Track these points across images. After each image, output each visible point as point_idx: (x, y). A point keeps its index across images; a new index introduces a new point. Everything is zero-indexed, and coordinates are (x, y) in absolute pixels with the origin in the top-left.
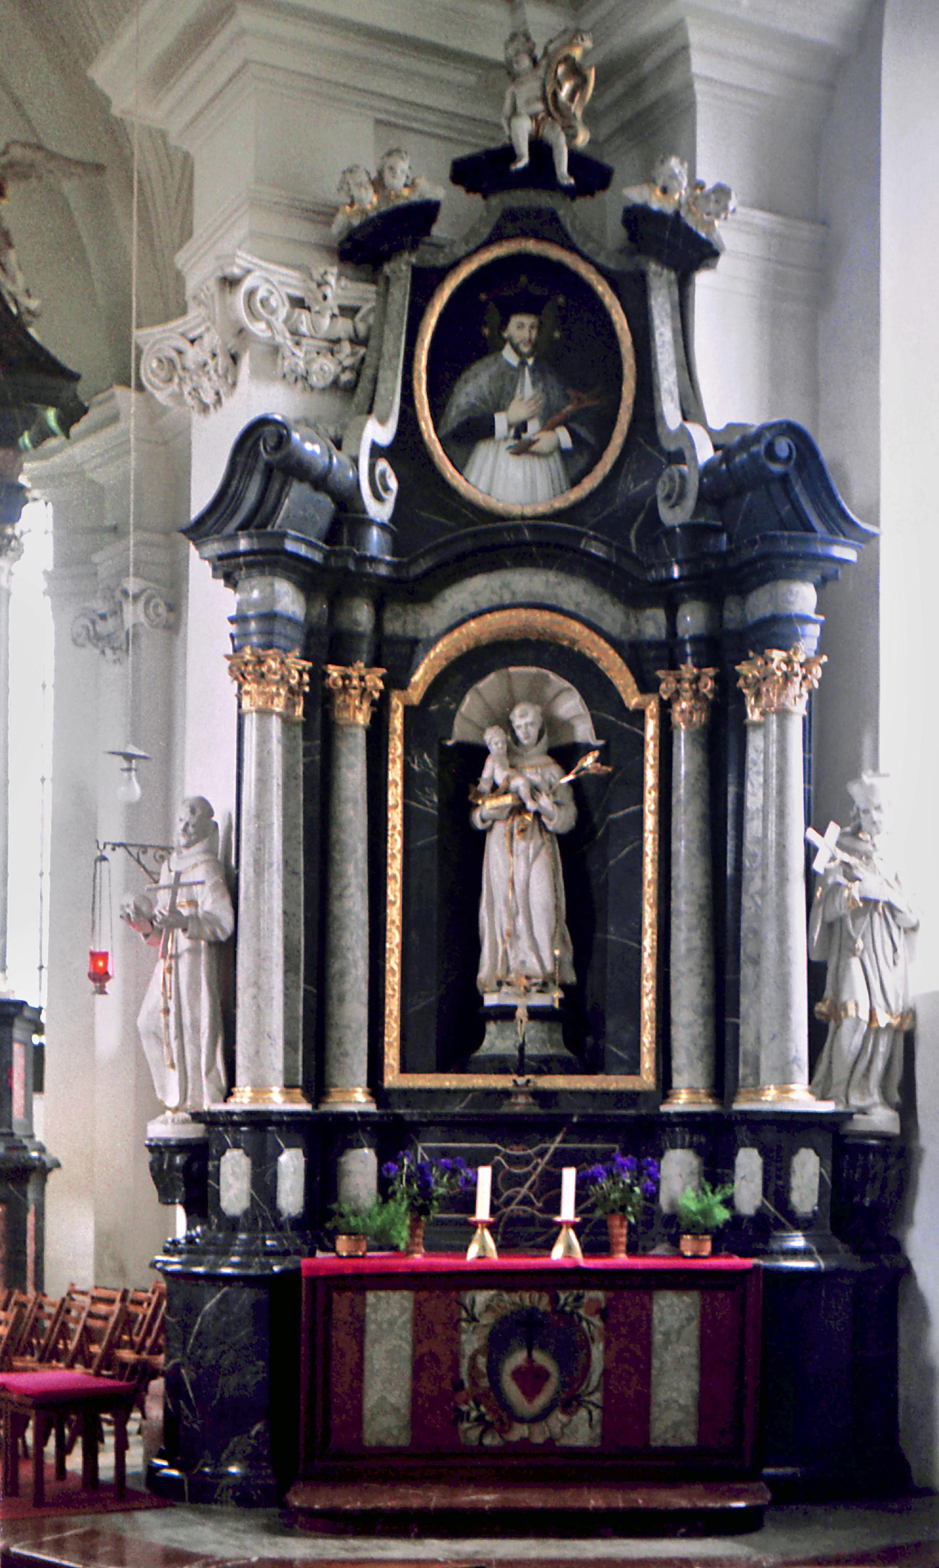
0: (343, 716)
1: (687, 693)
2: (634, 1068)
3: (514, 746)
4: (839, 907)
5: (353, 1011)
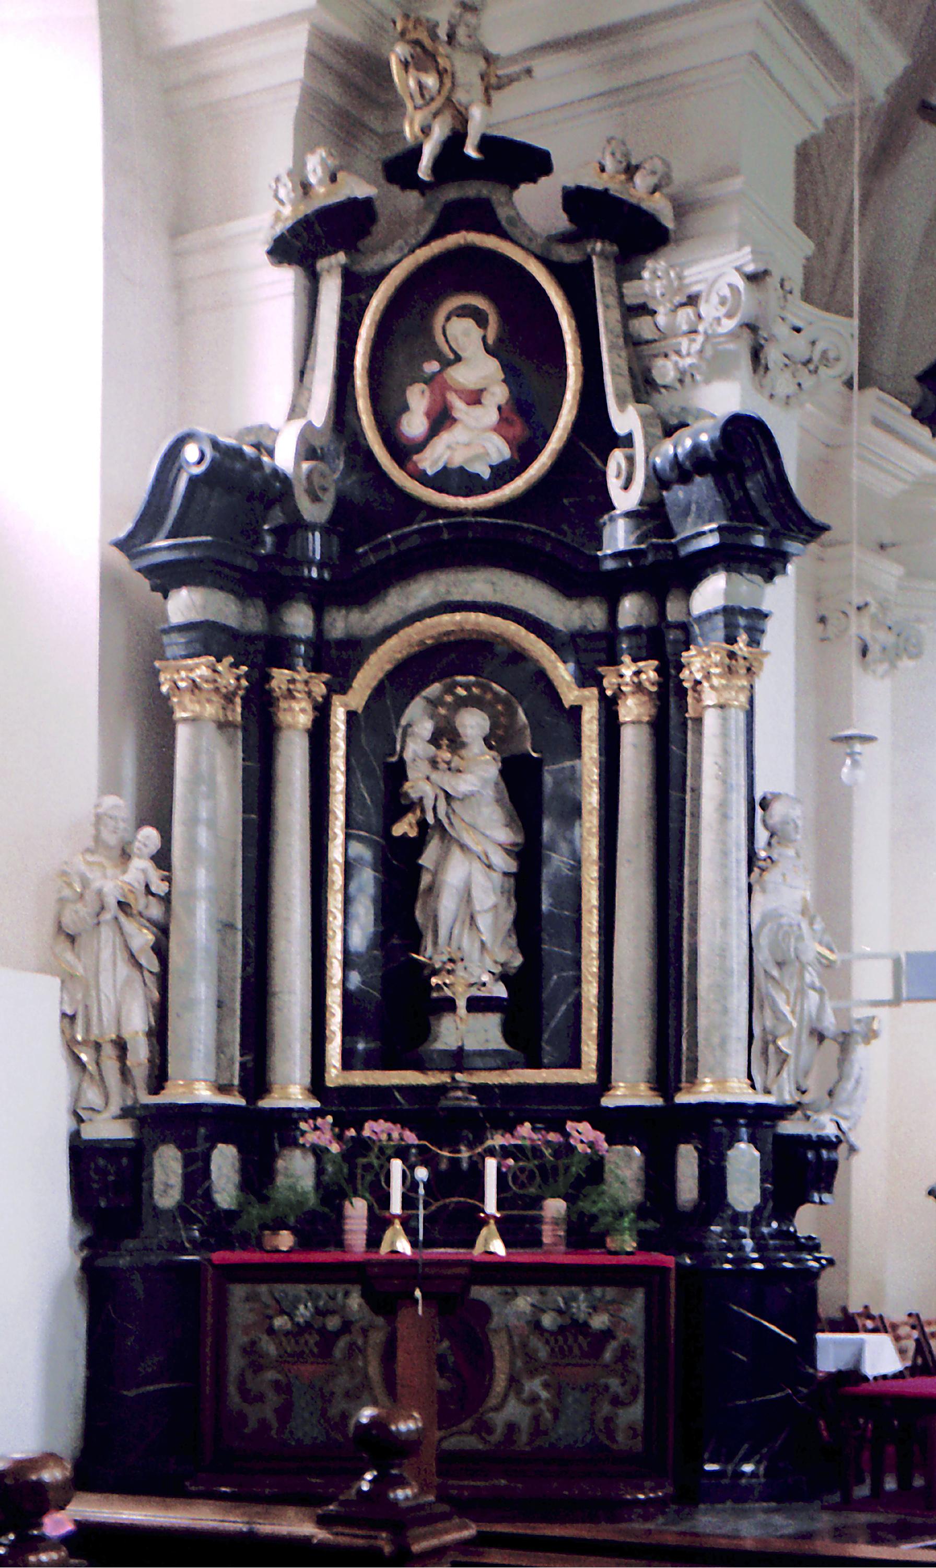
0: (284, 718)
1: (632, 674)
2: (575, 1062)
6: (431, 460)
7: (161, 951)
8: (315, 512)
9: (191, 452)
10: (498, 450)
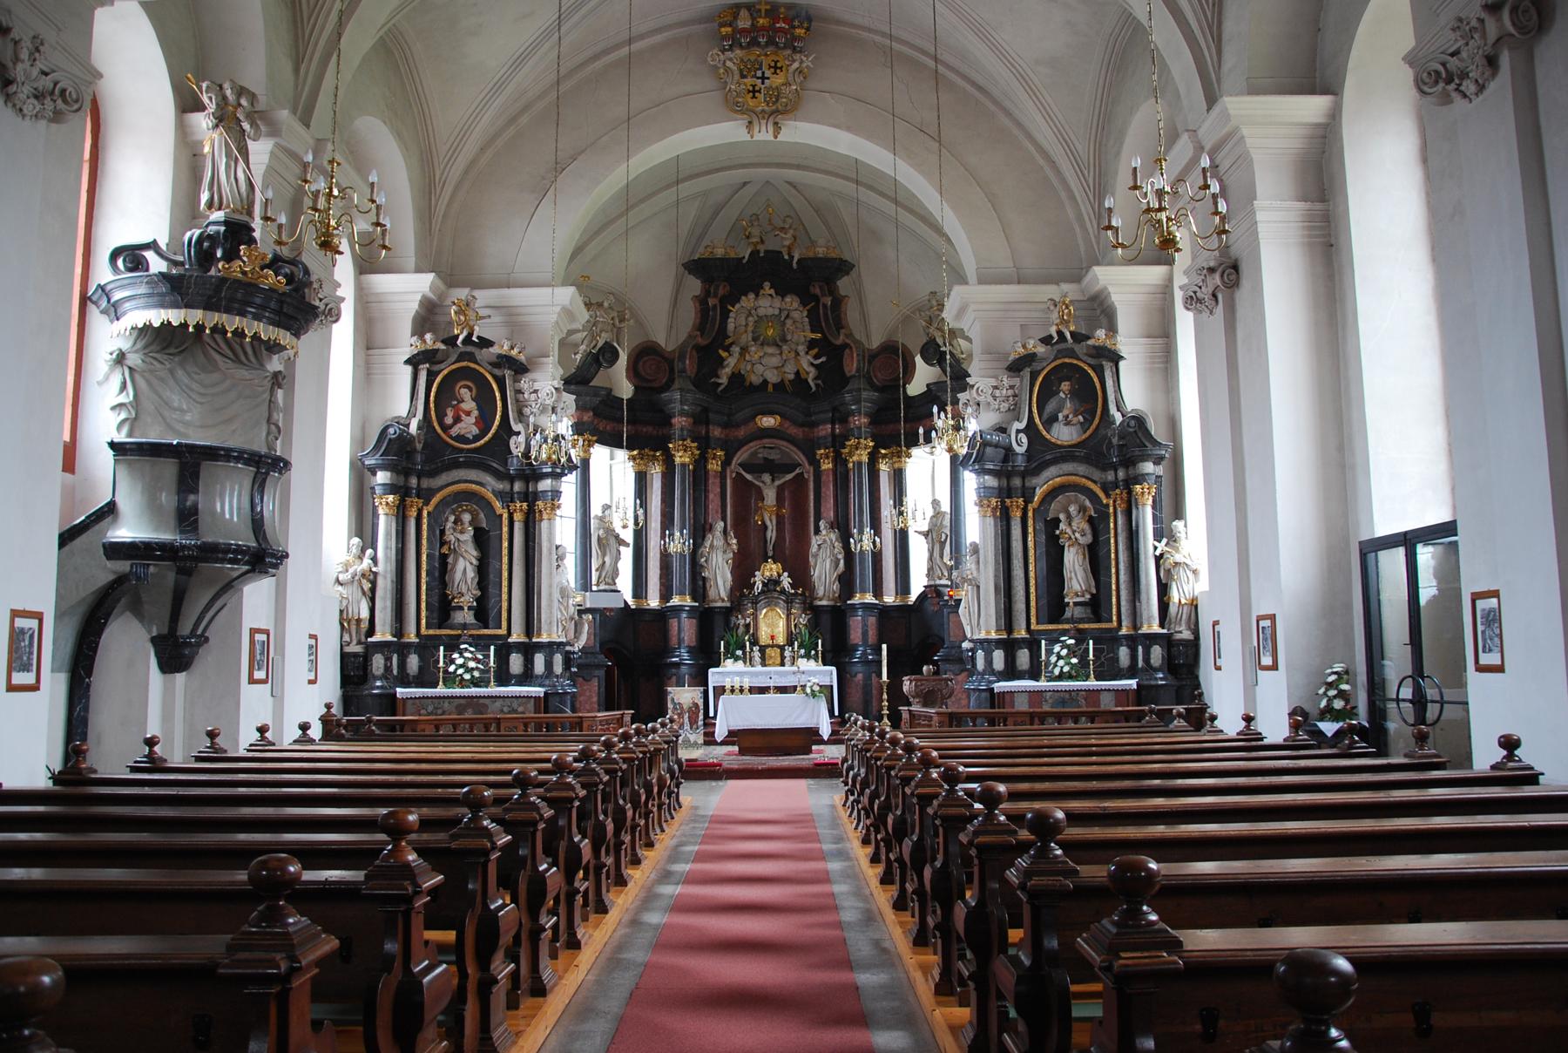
1: (520, 506)
2: (500, 627)
3: (1069, 518)
4: (1167, 566)
5: (1019, 606)
6: (455, 431)
7: (373, 590)
8: (419, 446)
9: (391, 431)
10: (475, 430)
